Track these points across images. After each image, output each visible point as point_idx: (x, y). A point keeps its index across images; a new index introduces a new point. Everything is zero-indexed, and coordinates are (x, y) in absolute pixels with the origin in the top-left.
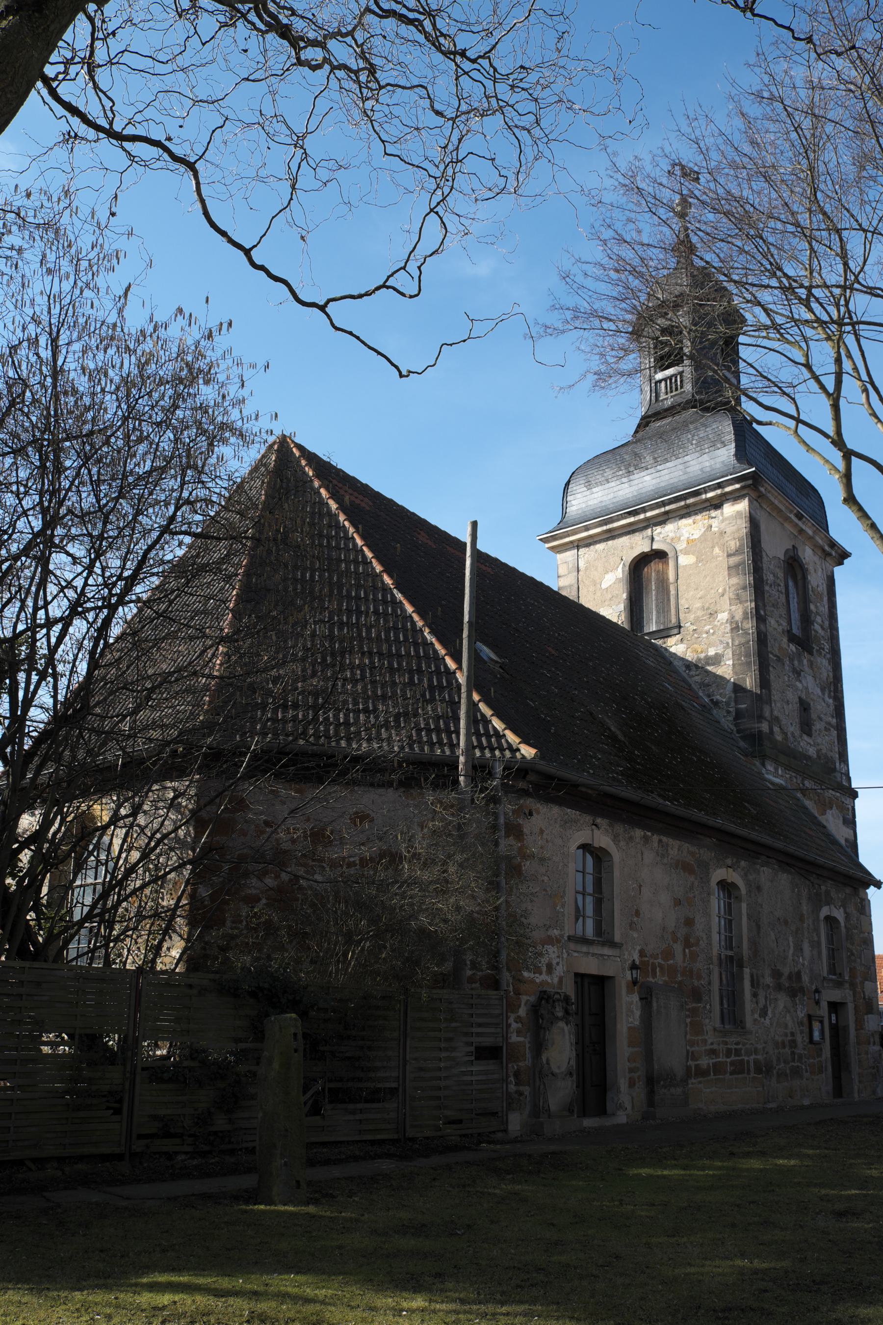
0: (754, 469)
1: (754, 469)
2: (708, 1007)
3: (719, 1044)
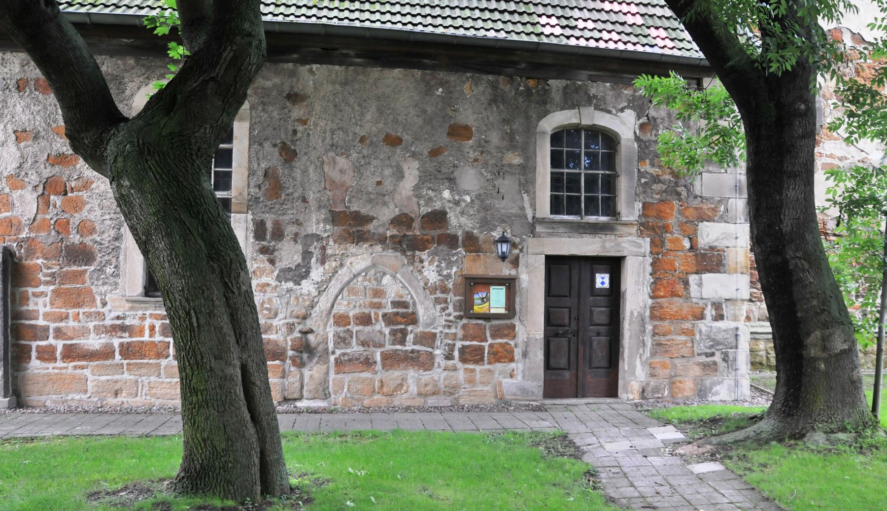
0: (221, 146)
1: (221, 146)
2: (109, 270)
3: (143, 318)
